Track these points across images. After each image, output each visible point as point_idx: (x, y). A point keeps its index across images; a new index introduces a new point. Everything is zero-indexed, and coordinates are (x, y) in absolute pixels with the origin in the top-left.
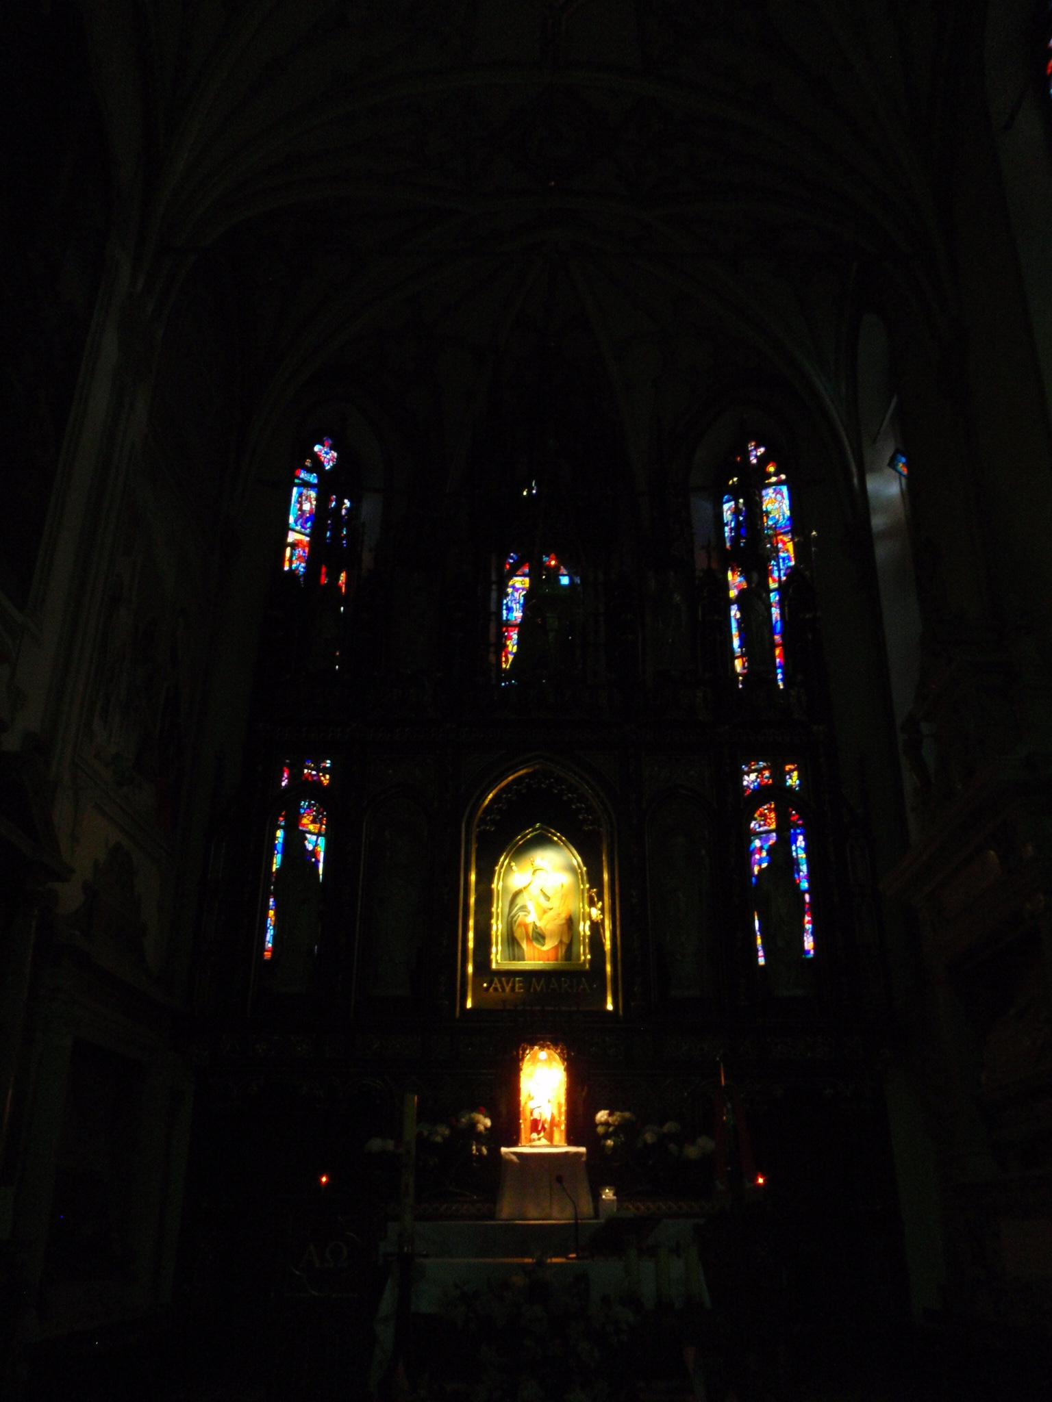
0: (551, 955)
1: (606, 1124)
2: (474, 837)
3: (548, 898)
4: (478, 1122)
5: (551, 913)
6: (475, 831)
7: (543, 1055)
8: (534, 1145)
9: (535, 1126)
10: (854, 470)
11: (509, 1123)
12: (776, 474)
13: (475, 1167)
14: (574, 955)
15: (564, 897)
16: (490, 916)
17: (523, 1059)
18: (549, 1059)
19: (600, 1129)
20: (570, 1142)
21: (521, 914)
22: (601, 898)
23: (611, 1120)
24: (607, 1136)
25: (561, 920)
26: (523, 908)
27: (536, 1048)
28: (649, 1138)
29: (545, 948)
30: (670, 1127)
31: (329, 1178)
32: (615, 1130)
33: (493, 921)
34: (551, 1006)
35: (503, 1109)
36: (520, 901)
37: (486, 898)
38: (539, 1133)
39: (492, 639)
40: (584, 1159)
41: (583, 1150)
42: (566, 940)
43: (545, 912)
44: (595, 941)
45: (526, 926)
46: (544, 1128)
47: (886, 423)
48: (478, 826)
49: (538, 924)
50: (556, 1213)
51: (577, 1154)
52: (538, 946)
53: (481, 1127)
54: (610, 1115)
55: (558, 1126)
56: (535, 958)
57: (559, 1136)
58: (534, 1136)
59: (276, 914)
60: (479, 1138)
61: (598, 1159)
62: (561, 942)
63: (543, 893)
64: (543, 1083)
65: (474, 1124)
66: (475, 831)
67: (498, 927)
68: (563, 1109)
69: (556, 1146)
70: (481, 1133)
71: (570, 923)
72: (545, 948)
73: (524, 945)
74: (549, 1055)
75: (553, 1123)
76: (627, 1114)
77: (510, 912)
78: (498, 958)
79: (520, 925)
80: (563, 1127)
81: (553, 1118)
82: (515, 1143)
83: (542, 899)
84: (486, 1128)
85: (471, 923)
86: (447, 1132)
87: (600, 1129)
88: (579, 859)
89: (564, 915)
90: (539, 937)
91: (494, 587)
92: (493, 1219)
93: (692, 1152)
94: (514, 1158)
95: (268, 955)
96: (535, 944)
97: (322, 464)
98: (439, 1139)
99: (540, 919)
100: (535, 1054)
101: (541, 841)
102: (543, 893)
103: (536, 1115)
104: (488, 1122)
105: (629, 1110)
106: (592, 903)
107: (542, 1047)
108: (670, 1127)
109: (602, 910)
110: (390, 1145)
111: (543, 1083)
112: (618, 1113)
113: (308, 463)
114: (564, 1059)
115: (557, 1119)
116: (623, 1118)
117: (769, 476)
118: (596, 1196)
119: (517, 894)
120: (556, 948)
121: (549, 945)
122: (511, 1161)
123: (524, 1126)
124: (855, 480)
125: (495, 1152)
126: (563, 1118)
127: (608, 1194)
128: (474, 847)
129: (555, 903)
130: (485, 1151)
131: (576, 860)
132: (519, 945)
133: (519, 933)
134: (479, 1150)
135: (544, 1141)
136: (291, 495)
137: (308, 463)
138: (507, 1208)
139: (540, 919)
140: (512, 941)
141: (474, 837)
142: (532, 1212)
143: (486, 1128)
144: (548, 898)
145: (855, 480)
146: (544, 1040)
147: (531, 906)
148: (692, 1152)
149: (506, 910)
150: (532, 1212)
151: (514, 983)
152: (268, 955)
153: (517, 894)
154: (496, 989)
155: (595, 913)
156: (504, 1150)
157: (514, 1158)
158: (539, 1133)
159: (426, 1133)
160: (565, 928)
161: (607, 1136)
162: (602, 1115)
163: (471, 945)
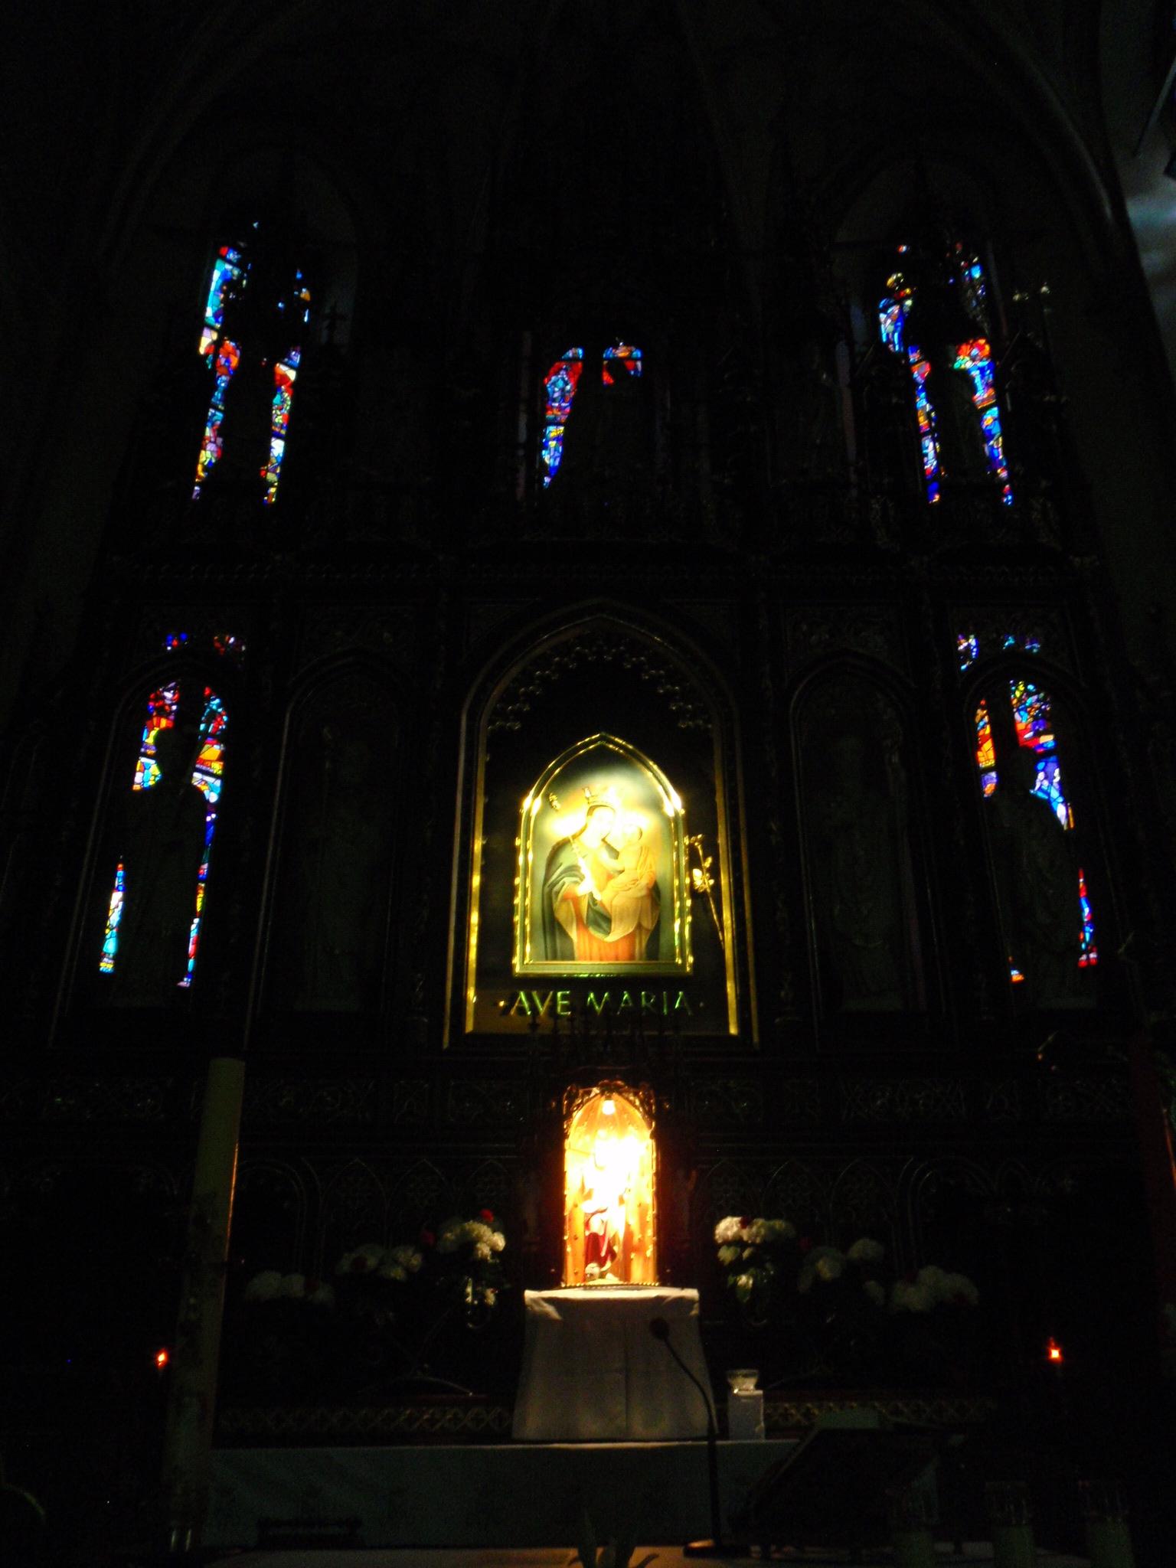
0: (623, 950)
1: (737, 1242)
2: (483, 740)
3: (615, 853)
4: (479, 1239)
5: (622, 878)
6: (485, 729)
7: (608, 1106)
8: (587, 1285)
9: (595, 1249)
10: (1104, 195)
11: (540, 1247)
13: (473, 1324)
14: (664, 949)
15: (644, 850)
17: (569, 1116)
18: (618, 1121)
19: (726, 1255)
20: (664, 1280)
21: (567, 880)
22: (711, 848)
23: (745, 1234)
24: (739, 1266)
25: (640, 890)
26: (573, 870)
27: (596, 1090)
28: (826, 1268)
30: (863, 1248)
31: (169, 1357)
32: (756, 1256)
33: (517, 918)
34: (624, 1033)
35: (530, 1215)
36: (566, 859)
37: (502, 865)
38: (602, 1263)
39: (523, 436)
40: (695, 1312)
41: (692, 1293)
42: (648, 924)
43: (610, 877)
44: (705, 937)
45: (576, 901)
46: (611, 1253)
47: (1154, 119)
48: (491, 722)
49: (598, 897)
50: (638, 1428)
51: (680, 1300)
52: (598, 935)
53: (485, 1250)
54: (744, 1224)
55: (640, 1249)
56: (593, 954)
57: (642, 1269)
58: (593, 1268)
59: (126, 900)
60: (477, 1269)
61: (718, 1317)
62: (639, 926)
63: (607, 842)
64: (610, 1166)
65: (469, 1244)
66: (485, 729)
67: (526, 900)
68: (651, 1214)
69: (637, 1287)
70: (484, 1260)
71: (655, 894)
73: (573, 933)
74: (621, 1111)
75: (629, 1246)
76: (778, 1224)
77: (546, 879)
78: (525, 959)
79: (565, 899)
80: (650, 1251)
81: (629, 1235)
82: (555, 1282)
83: (605, 855)
84: (495, 1252)
85: (474, 918)
86: (416, 1261)
87: (726, 1255)
89: (644, 882)
90: (601, 919)
91: (522, 407)
92: (507, 1437)
93: (913, 1296)
94: (550, 1309)
96: (592, 931)
98: (398, 1273)
99: (602, 889)
100: (594, 1109)
101: (603, 761)
102: (607, 842)
103: (596, 1227)
104: (500, 1241)
105: (778, 1216)
106: (694, 862)
107: (608, 1091)
108: (863, 1248)
109: (714, 872)
111: (610, 1166)
112: (760, 1221)
114: (649, 1115)
115: (637, 1236)
116: (771, 1229)
118: (722, 1390)
119: (559, 848)
120: (631, 937)
121: (618, 932)
122: (546, 1316)
123: (574, 1250)
124: (1108, 211)
125: (512, 1300)
126: (650, 1232)
127: (745, 1387)
128: (483, 759)
129: (628, 861)
130: (491, 1297)
132: (564, 934)
133: (562, 913)
134: (479, 1295)
135: (611, 1279)
136: (210, 280)
138: (534, 1419)
139: (602, 889)
140: (551, 926)
141: (483, 740)
142: (589, 1423)
143: (495, 1252)
144: (615, 853)
145: (1108, 211)
146: (612, 1075)
147: (585, 869)
148: (913, 1296)
149: (541, 873)
150: (589, 1423)
151: (554, 997)
153: (559, 848)
154: (521, 1011)
155: (701, 879)
156: (530, 1294)
157: (550, 1309)
158: (602, 1263)
159: (372, 1262)
160: (648, 903)
161: (739, 1266)
162: (728, 1227)
163: (473, 954)
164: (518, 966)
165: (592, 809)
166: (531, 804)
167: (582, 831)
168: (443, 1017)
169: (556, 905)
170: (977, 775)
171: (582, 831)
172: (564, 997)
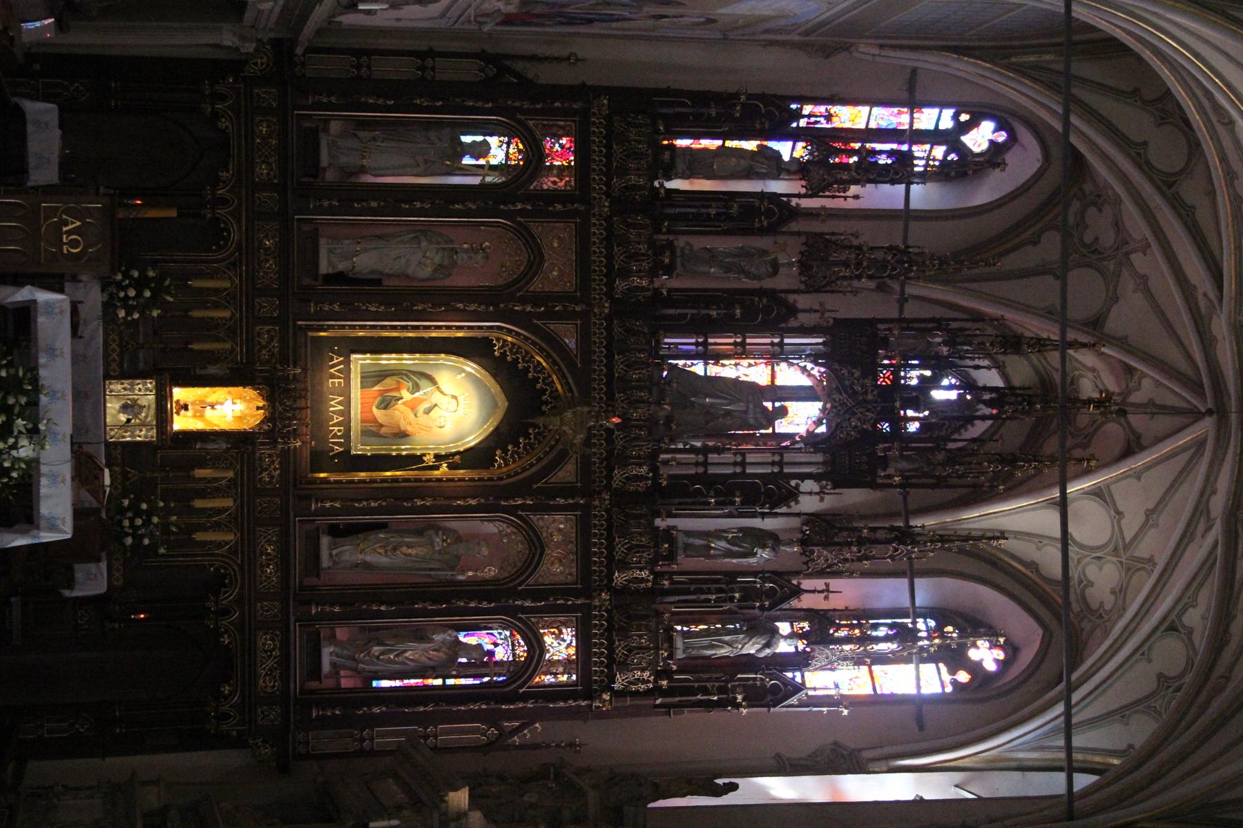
2: (487, 334)
5: (412, 416)
6: (493, 335)
12: (955, 683)
16: (411, 351)
25: (404, 426)
29: (374, 409)
36: (423, 382)
43: (413, 409)
45: (398, 389)
48: (498, 339)
62: (382, 426)
72: (374, 409)
83: (426, 405)
88: (472, 444)
89: (409, 429)
95: (375, 684)
97: (966, 132)
110: (44, 173)
113: (964, 117)
117: (953, 671)
131: (472, 441)
133: (389, 382)
137: (964, 117)
143: (975, 645)
144: (428, 411)
152: (375, 684)
153: (432, 381)
160: (396, 431)
164: (354, 356)
165: (455, 397)
166: (470, 367)
167: (442, 392)
168: (372, 338)
169: (396, 378)
170: (382, 712)
171: (442, 392)
172: (340, 383)
